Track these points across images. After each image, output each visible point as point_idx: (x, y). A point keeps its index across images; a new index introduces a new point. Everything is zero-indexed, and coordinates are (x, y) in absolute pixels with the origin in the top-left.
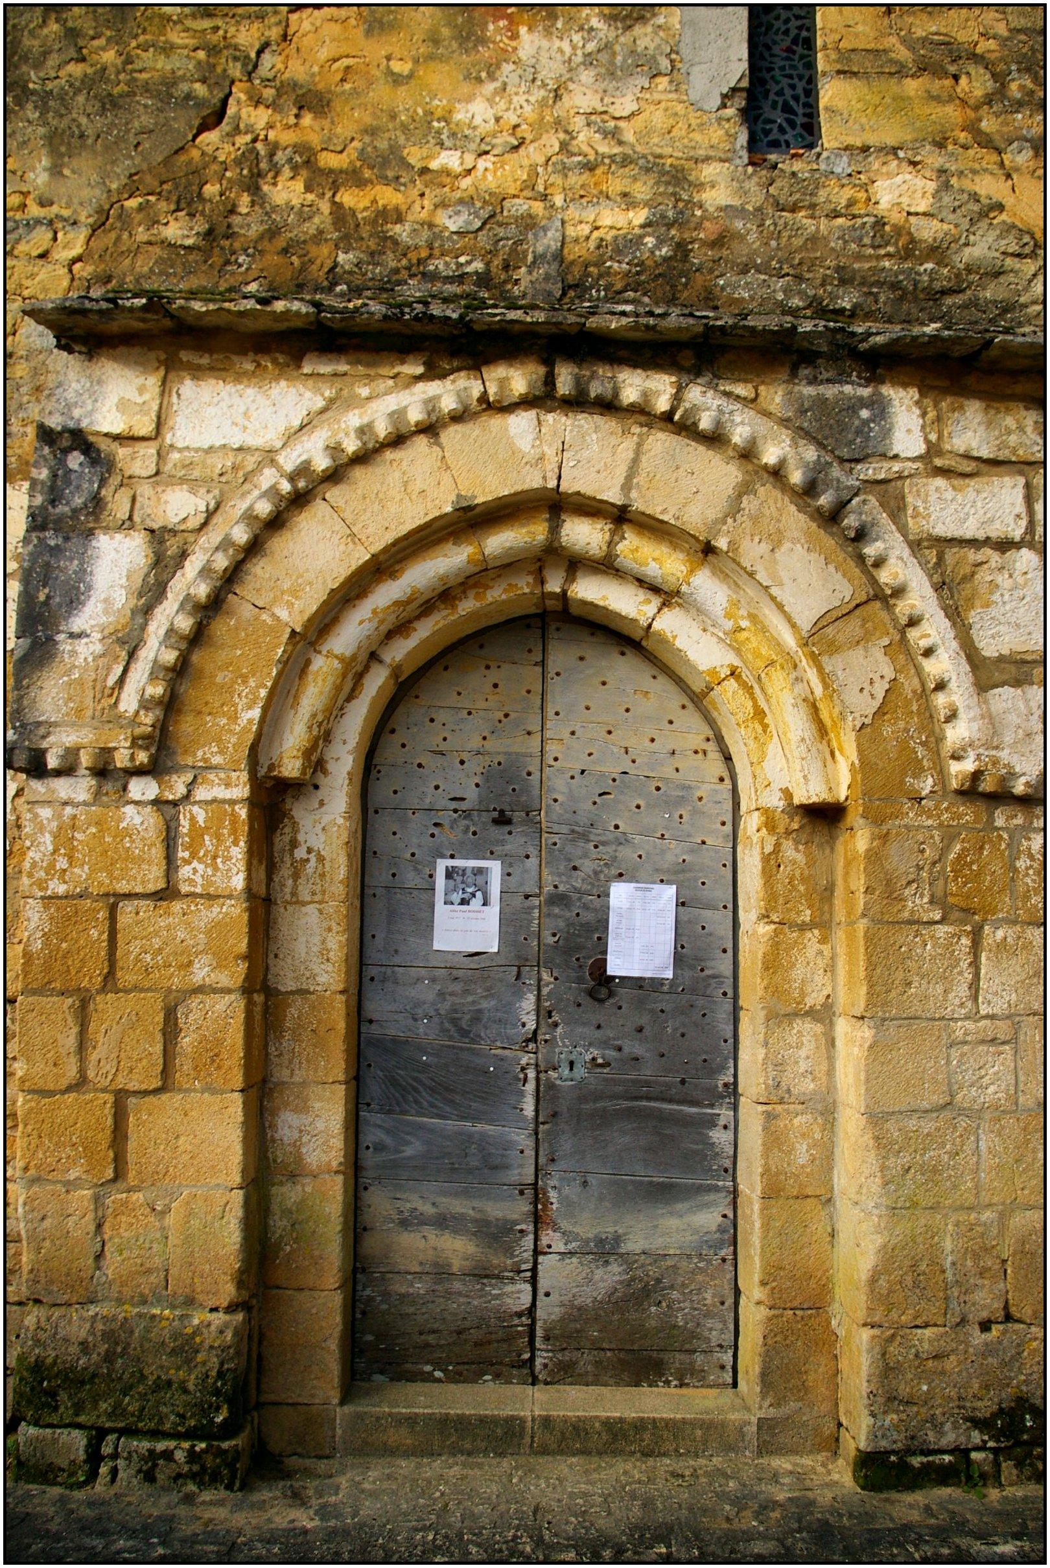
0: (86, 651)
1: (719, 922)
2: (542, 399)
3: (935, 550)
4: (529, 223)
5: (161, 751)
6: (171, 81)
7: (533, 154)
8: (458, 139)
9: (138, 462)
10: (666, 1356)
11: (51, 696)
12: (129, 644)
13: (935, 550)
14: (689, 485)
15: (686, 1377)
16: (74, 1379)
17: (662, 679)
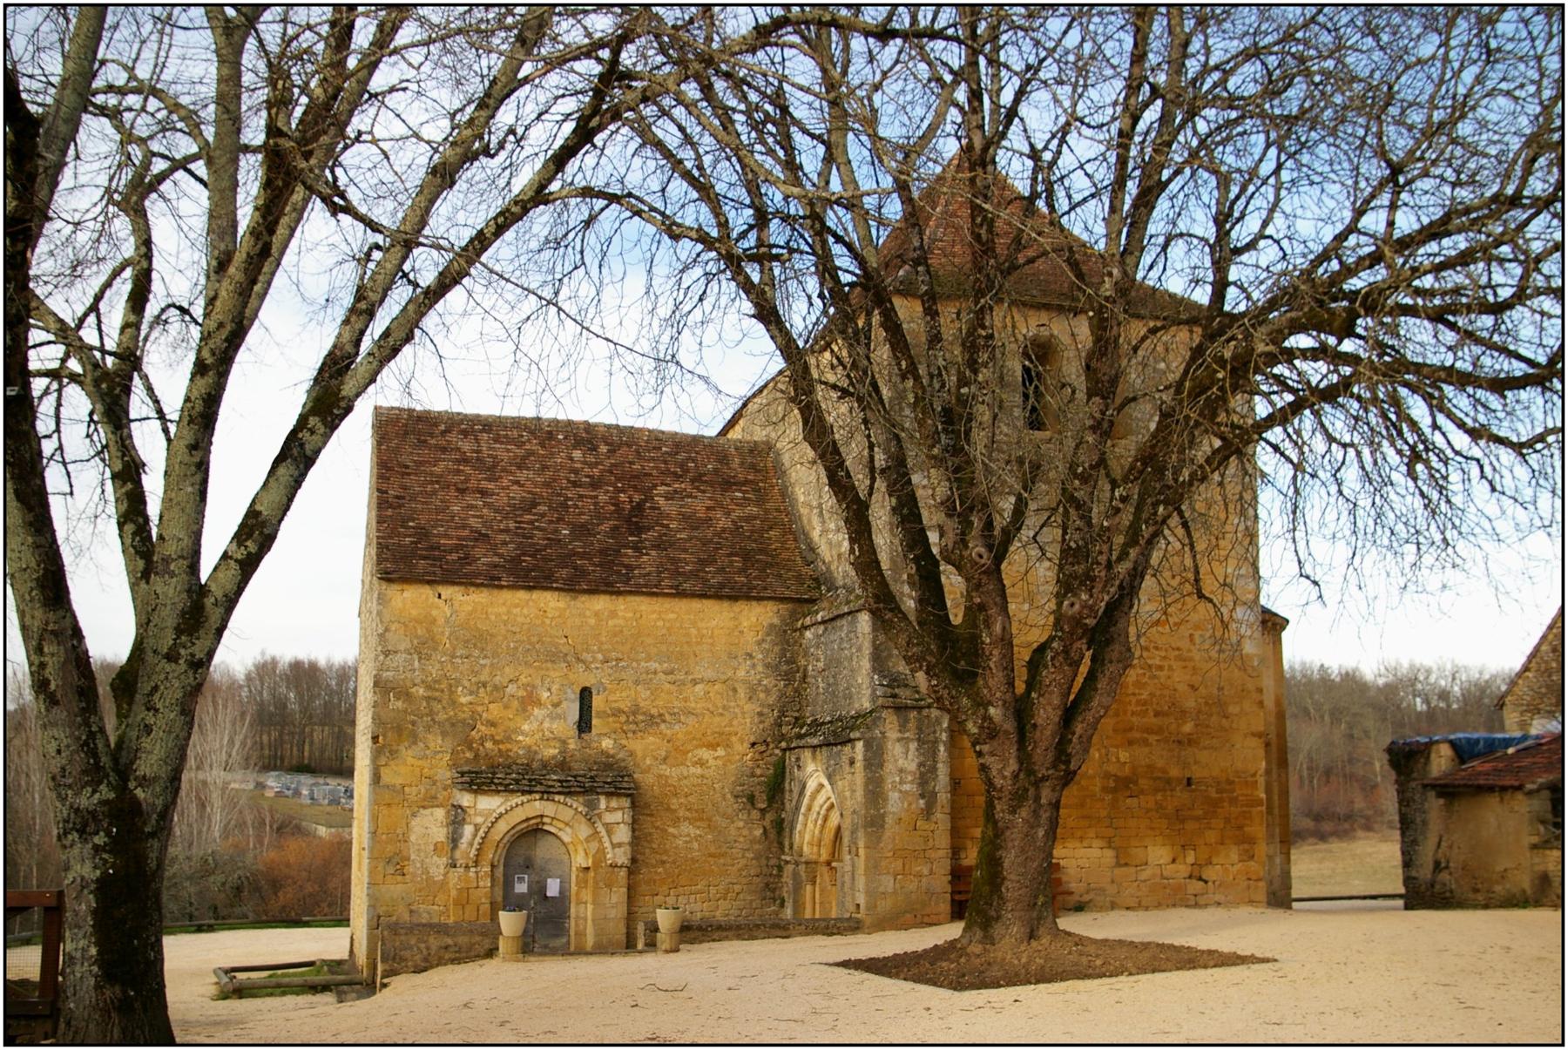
3: (606, 825)
5: (476, 863)
8: (523, 733)
9: (471, 812)
11: (458, 854)
12: (471, 844)
13: (606, 825)
14: (566, 814)
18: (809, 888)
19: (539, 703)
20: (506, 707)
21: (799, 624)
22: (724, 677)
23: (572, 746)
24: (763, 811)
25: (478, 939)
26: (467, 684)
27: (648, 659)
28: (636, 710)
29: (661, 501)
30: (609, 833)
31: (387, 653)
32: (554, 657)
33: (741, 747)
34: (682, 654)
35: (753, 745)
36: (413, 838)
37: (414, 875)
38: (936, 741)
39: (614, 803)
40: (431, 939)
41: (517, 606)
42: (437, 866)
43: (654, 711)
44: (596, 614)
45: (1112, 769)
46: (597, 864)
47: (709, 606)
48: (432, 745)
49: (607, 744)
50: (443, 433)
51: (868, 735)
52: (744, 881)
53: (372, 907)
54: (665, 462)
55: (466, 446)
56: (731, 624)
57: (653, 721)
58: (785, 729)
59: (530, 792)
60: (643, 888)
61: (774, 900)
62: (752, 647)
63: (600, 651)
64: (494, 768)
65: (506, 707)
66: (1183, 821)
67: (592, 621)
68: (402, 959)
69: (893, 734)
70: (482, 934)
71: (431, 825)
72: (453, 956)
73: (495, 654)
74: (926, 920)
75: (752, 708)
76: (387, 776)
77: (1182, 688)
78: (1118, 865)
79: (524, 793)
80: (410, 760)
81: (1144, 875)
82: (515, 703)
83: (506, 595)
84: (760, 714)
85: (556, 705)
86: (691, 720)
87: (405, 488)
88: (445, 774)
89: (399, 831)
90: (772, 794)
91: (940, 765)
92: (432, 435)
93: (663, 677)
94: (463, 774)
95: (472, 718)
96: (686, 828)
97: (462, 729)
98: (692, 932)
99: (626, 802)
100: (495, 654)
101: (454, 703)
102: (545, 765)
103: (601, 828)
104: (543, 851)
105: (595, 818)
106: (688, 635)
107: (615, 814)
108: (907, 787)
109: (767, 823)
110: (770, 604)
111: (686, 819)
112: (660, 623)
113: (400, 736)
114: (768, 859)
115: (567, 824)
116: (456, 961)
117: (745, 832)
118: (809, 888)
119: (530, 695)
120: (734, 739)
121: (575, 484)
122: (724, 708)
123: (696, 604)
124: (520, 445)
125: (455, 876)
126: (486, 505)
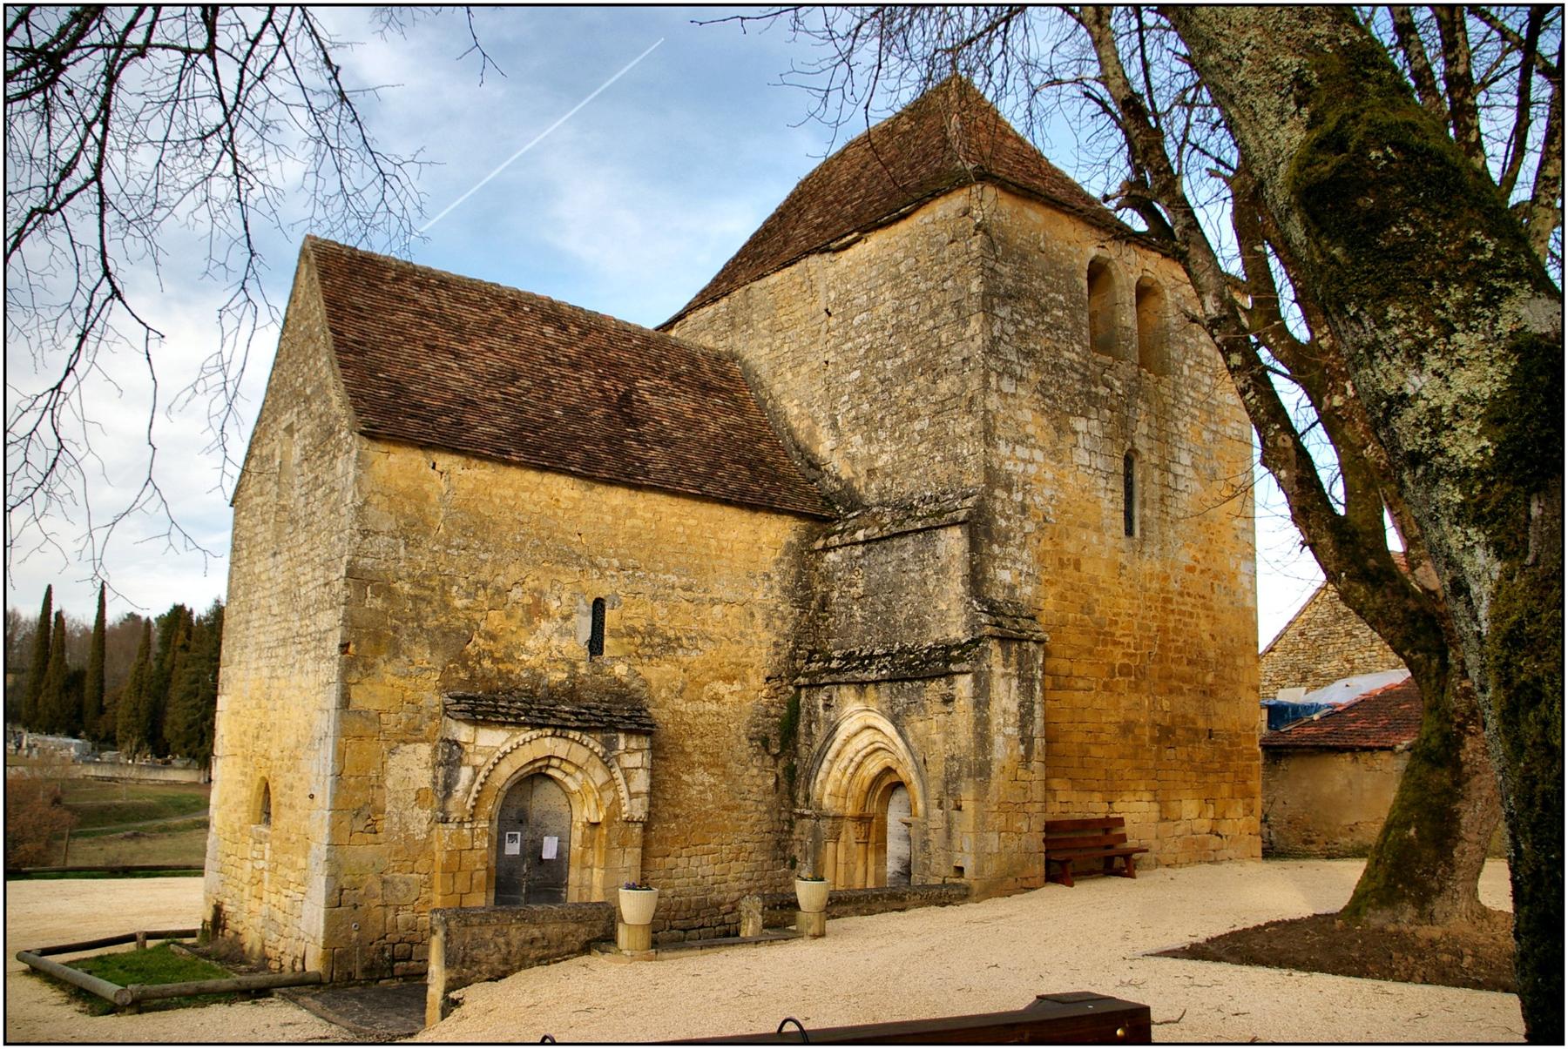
0: (459, 795)
1: (566, 845)
2: (553, 735)
4: (541, 676)
6: (459, 628)
7: (542, 656)
8: (527, 651)
9: (470, 749)
11: (451, 805)
14: (579, 755)
17: (77, 340)
18: (830, 846)
19: (547, 615)
20: (509, 616)
21: (819, 544)
22: (742, 599)
23: (582, 671)
24: (776, 757)
25: (572, 927)
26: (463, 583)
27: (667, 570)
28: (651, 631)
29: (647, 396)
30: (627, 779)
31: (365, 534)
32: (566, 558)
33: (756, 682)
34: (700, 567)
35: (768, 679)
36: (389, 783)
37: (389, 832)
38: (1032, 680)
39: (633, 744)
40: (513, 931)
41: (526, 489)
42: (420, 820)
43: (671, 634)
44: (614, 510)
45: (1158, 718)
46: (610, 819)
47: (729, 513)
48: (417, 659)
49: (620, 670)
50: (396, 280)
51: (976, 669)
52: (757, 838)
53: (332, 877)
54: (640, 355)
55: (425, 299)
56: (751, 538)
57: (670, 645)
58: (799, 663)
59: (541, 726)
60: (655, 847)
61: (784, 859)
62: (769, 567)
63: (616, 555)
64: (492, 693)
65: (509, 616)
66: (1206, 774)
67: (609, 519)
68: (475, 962)
69: (998, 669)
70: (578, 921)
71: (413, 767)
72: (539, 953)
73: (499, 548)
74: (1025, 884)
75: (768, 637)
76: (359, 699)
77: (1206, 636)
78: (1163, 819)
79: (534, 726)
80: (389, 678)
81: (1179, 830)
82: (520, 612)
83: (514, 474)
84: (776, 644)
85: (566, 618)
86: (709, 647)
87: (363, 333)
88: (432, 699)
89: (373, 773)
90: (788, 740)
91: (1037, 707)
92: (382, 280)
93: (682, 593)
94: (459, 700)
95: (468, 627)
96: (702, 777)
97: (453, 641)
98: (841, 904)
99: (645, 743)
100: (499, 548)
101: (446, 606)
102: (551, 692)
103: (618, 774)
104: (544, 800)
105: (614, 761)
106: (707, 546)
107: (633, 756)
108: (1010, 730)
109: (779, 771)
110: (790, 519)
111: (701, 764)
112: (680, 529)
113: (378, 644)
114: (780, 812)
115: (578, 767)
116: (544, 960)
117: (759, 781)
118: (830, 846)
119: (537, 603)
120: (750, 671)
121: (554, 362)
122: (742, 634)
123: (718, 511)
124: (486, 310)
125: (445, 833)
126: (461, 368)
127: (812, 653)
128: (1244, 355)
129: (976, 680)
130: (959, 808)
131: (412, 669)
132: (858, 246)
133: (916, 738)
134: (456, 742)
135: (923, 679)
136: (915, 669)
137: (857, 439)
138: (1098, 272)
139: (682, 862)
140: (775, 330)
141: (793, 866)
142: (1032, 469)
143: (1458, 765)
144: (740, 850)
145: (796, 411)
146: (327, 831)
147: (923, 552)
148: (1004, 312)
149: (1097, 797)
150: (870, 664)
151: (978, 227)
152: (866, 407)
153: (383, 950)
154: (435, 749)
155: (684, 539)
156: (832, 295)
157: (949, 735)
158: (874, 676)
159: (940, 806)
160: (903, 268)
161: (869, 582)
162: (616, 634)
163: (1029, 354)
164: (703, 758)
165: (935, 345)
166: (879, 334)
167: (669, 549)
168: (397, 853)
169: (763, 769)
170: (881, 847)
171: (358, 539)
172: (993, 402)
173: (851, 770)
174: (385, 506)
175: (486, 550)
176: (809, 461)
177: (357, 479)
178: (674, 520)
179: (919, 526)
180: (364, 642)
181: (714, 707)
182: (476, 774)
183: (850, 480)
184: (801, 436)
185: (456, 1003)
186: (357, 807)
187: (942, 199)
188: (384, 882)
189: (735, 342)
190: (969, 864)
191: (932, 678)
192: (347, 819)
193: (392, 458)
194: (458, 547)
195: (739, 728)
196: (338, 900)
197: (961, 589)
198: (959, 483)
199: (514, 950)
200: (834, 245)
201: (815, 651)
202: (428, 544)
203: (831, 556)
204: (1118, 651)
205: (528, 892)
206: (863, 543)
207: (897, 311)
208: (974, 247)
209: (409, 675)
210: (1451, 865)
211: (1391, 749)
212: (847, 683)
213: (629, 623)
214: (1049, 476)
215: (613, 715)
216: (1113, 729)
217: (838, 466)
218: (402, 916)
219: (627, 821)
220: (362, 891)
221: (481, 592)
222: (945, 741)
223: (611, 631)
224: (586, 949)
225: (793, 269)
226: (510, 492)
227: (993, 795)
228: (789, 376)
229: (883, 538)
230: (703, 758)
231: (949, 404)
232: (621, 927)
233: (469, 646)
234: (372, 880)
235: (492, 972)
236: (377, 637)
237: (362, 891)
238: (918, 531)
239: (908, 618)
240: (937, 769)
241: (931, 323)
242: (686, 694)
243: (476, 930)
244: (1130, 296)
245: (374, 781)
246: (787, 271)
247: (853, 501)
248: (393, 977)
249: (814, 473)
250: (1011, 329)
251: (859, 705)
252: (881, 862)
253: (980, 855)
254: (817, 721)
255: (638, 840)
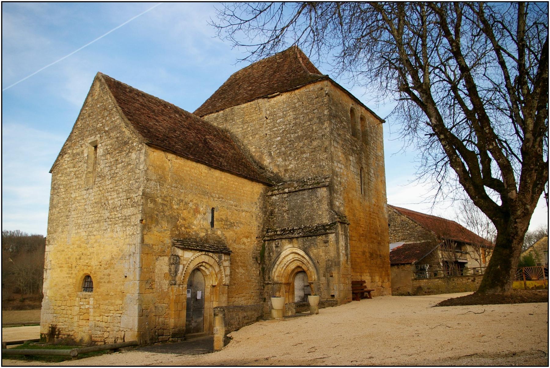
8: (194, 225)
9: (182, 258)
10: (416, 277)
15: (201, 332)
16: (177, 334)
19: (199, 212)
20: (189, 212)
21: (270, 193)
22: (250, 210)
23: (209, 233)
24: (259, 264)
25: (254, 312)
32: (205, 193)
33: (254, 238)
36: (156, 271)
43: (232, 221)
44: (216, 178)
46: (219, 284)
48: (163, 226)
49: (219, 233)
52: (255, 291)
53: (140, 305)
56: (251, 190)
71: (163, 265)
75: (256, 223)
76: (147, 241)
78: (372, 282)
82: (192, 211)
86: (241, 226)
88: (168, 241)
89: (151, 267)
90: (264, 260)
94: (178, 241)
97: (173, 219)
98: (322, 304)
100: (186, 189)
103: (222, 268)
106: (240, 192)
112: (234, 186)
115: (211, 266)
119: (197, 208)
127: (268, 229)
128: (444, 135)
129: (336, 235)
130: (332, 276)
131: (162, 230)
132: (279, 97)
133: (314, 255)
134: (178, 256)
135: (315, 236)
136: (312, 233)
137: (280, 159)
138: (352, 111)
139: (236, 299)
140: (244, 123)
141: (264, 301)
142: (342, 171)
143: (511, 248)
144: (251, 296)
145: (254, 150)
146: (138, 288)
147: (311, 195)
148: (333, 121)
149: (358, 274)
150: (294, 232)
151: (327, 94)
152: (283, 149)
153: (155, 332)
154: (170, 259)
155: (234, 189)
156: (268, 112)
157: (326, 253)
158: (297, 236)
159: (324, 276)
160: (297, 105)
161: (290, 205)
162: (217, 220)
163: (339, 135)
164: (241, 264)
165: (311, 130)
166: (288, 126)
167: (231, 192)
168: (159, 296)
169: (256, 268)
170: (293, 294)
171: (145, 182)
172: (333, 149)
173: (284, 268)
174: (153, 171)
175: (182, 189)
176: (260, 167)
177: (145, 160)
178: (232, 182)
179: (310, 187)
180: (148, 219)
181: (243, 247)
182: (184, 267)
183: (277, 173)
184: (257, 158)
185: (231, 338)
186: (147, 280)
187: (313, 84)
188: (156, 307)
189: (227, 126)
190: (336, 294)
191: (319, 235)
192: (144, 284)
193: (155, 154)
194: (174, 187)
195: (250, 254)
196: (143, 314)
197: (327, 207)
198: (322, 174)
199: (240, 320)
200: (269, 96)
201: (269, 229)
202: (166, 185)
203: (274, 197)
204: (361, 229)
205: (193, 311)
206: (287, 193)
207: (295, 119)
208: (325, 100)
209: (161, 232)
210: (509, 275)
211: (411, 264)
212: (286, 238)
213: (221, 217)
214: (345, 173)
215: (220, 249)
216: (360, 253)
217: (272, 168)
218: (161, 319)
219: (224, 285)
220: (149, 311)
221: (181, 203)
222: (326, 255)
223: (217, 219)
224: (257, 320)
225: (252, 103)
226: (188, 169)
227: (341, 273)
228: (251, 138)
229: (296, 191)
230: (241, 264)
231: (317, 149)
232: (273, 311)
233: (178, 222)
234: (151, 306)
235: (235, 328)
236: (151, 217)
237: (149, 311)
238: (310, 189)
239: (307, 217)
240: (323, 264)
241: (309, 123)
242: (236, 242)
243: (231, 313)
244: (359, 120)
245: (152, 270)
246: (249, 103)
247: (279, 179)
248: (159, 342)
249: (262, 170)
250: (335, 127)
251: (290, 246)
252: (293, 298)
253: (340, 291)
254: (273, 252)
255: (226, 292)
